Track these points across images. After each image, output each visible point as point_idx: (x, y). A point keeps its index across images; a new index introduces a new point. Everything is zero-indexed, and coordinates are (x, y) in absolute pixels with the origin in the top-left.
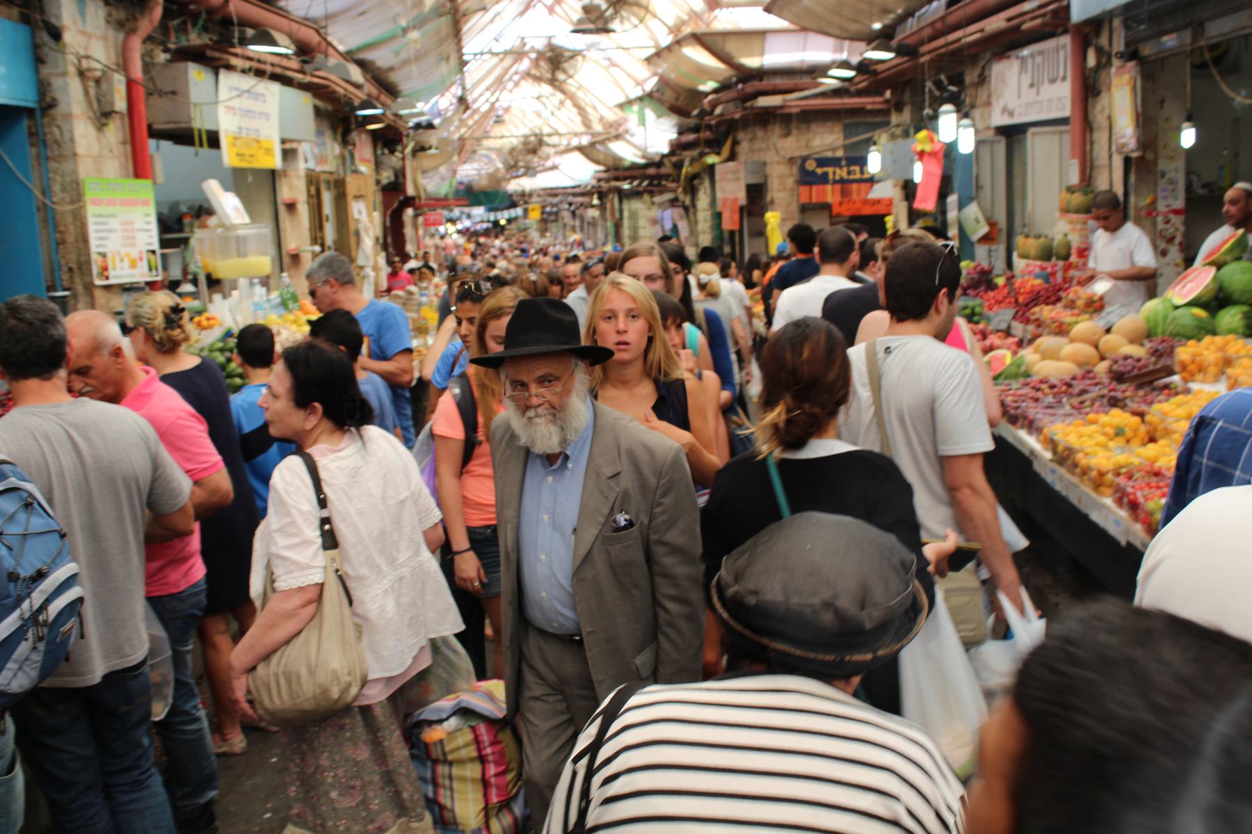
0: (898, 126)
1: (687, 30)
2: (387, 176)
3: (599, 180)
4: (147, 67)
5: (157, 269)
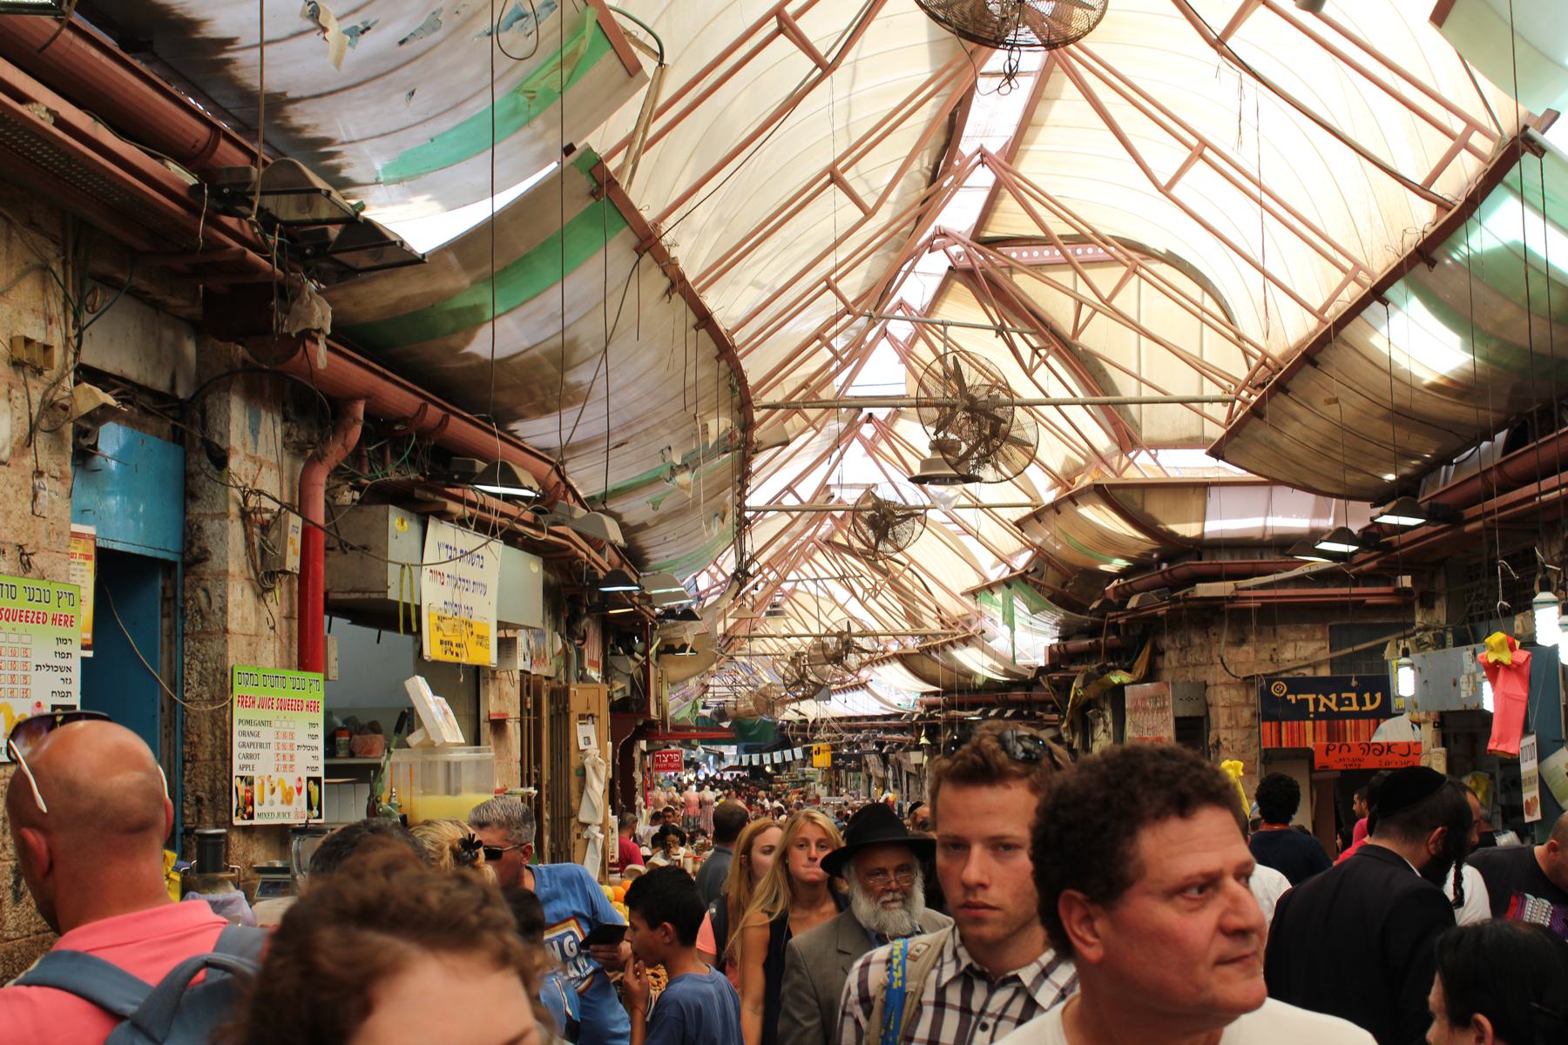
0: (1426, 629)
1: (1082, 481)
2: (621, 687)
3: (930, 707)
4: (331, 509)
5: (319, 808)
